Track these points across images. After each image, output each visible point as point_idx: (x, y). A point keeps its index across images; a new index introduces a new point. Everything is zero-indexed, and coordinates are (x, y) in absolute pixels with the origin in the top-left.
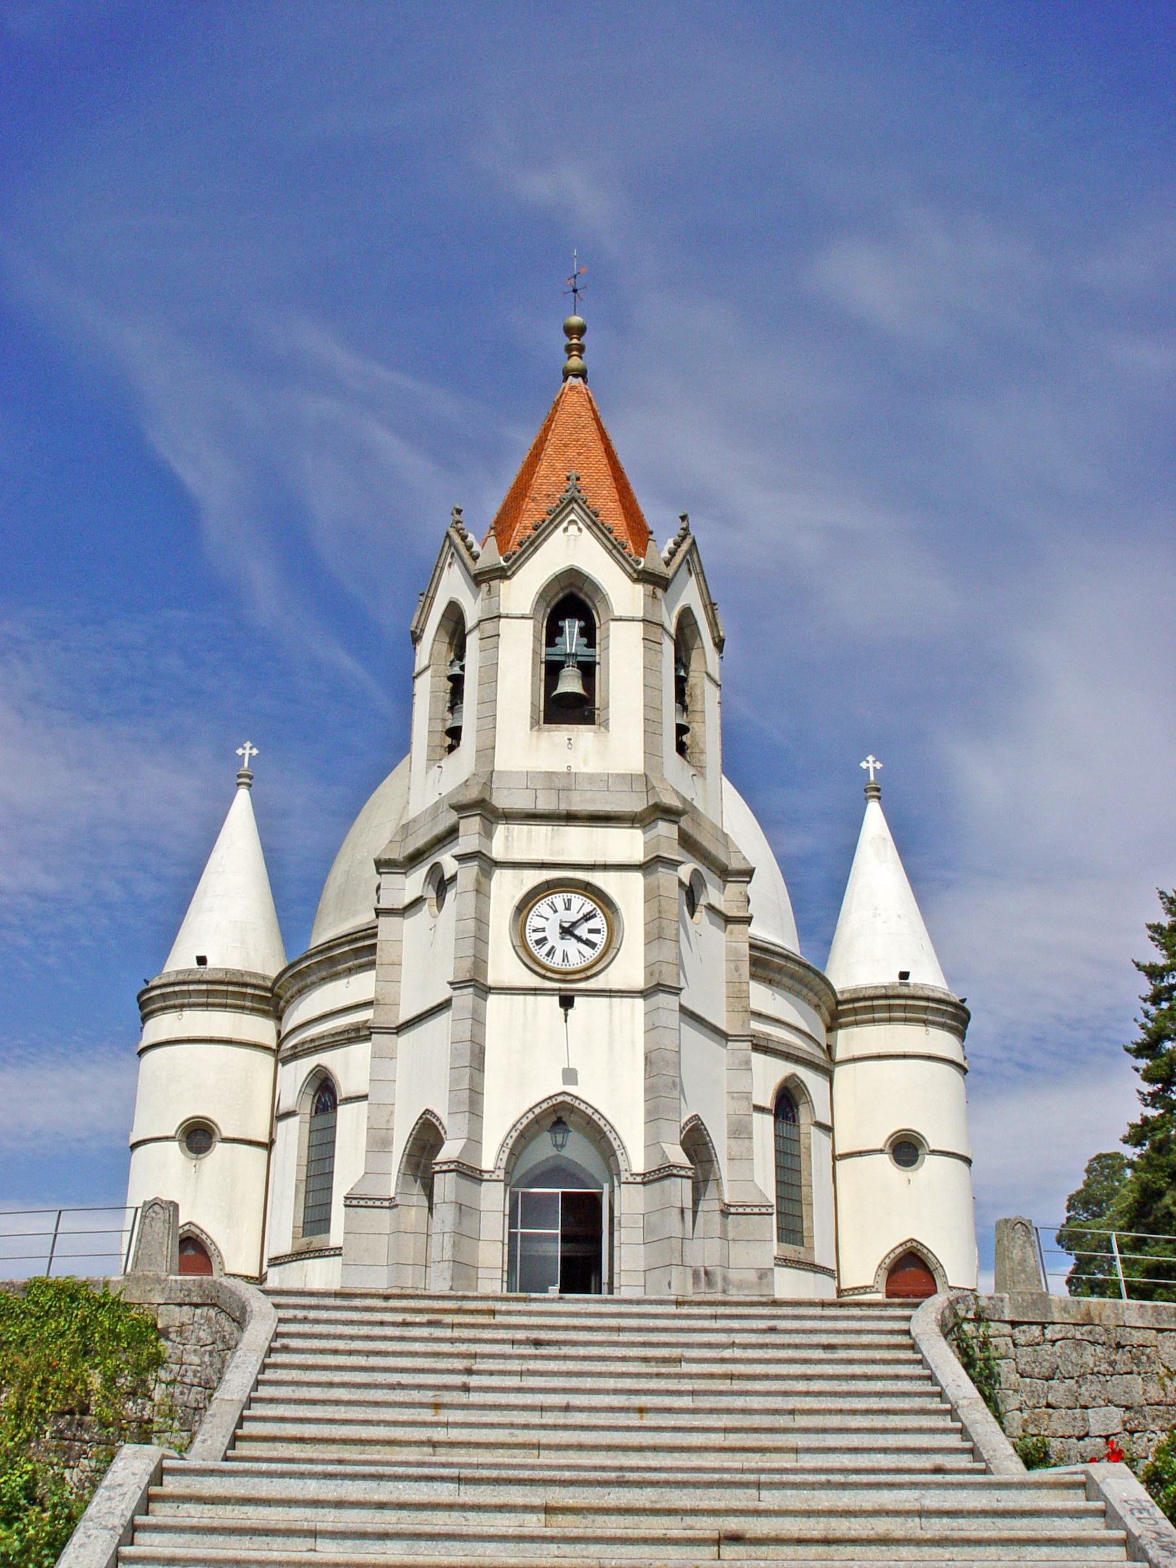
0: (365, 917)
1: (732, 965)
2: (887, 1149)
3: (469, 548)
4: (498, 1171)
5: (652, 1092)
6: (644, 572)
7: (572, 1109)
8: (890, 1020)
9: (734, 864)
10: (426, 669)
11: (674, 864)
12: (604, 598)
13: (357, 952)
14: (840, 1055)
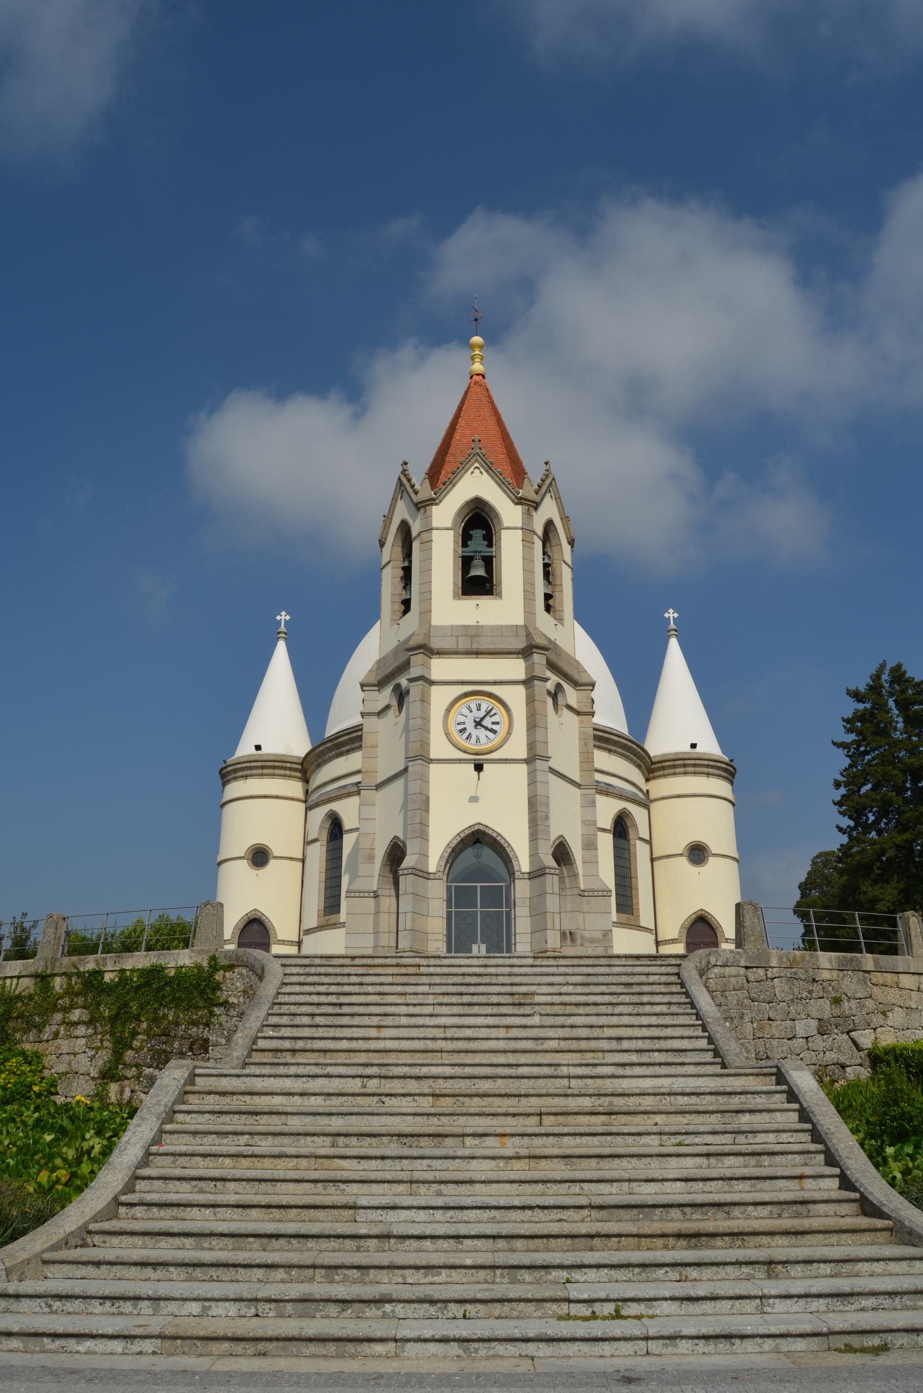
0: (356, 720)
1: (583, 742)
2: (686, 854)
3: (412, 486)
4: (439, 874)
5: (534, 823)
6: (521, 498)
7: (484, 834)
8: (685, 773)
9: (583, 679)
10: (389, 562)
11: (546, 680)
12: (497, 515)
13: (351, 741)
14: (652, 797)
